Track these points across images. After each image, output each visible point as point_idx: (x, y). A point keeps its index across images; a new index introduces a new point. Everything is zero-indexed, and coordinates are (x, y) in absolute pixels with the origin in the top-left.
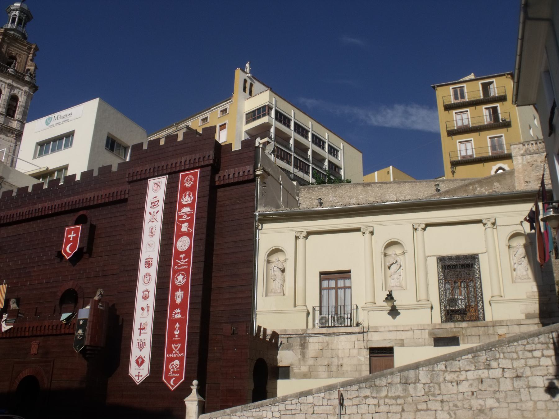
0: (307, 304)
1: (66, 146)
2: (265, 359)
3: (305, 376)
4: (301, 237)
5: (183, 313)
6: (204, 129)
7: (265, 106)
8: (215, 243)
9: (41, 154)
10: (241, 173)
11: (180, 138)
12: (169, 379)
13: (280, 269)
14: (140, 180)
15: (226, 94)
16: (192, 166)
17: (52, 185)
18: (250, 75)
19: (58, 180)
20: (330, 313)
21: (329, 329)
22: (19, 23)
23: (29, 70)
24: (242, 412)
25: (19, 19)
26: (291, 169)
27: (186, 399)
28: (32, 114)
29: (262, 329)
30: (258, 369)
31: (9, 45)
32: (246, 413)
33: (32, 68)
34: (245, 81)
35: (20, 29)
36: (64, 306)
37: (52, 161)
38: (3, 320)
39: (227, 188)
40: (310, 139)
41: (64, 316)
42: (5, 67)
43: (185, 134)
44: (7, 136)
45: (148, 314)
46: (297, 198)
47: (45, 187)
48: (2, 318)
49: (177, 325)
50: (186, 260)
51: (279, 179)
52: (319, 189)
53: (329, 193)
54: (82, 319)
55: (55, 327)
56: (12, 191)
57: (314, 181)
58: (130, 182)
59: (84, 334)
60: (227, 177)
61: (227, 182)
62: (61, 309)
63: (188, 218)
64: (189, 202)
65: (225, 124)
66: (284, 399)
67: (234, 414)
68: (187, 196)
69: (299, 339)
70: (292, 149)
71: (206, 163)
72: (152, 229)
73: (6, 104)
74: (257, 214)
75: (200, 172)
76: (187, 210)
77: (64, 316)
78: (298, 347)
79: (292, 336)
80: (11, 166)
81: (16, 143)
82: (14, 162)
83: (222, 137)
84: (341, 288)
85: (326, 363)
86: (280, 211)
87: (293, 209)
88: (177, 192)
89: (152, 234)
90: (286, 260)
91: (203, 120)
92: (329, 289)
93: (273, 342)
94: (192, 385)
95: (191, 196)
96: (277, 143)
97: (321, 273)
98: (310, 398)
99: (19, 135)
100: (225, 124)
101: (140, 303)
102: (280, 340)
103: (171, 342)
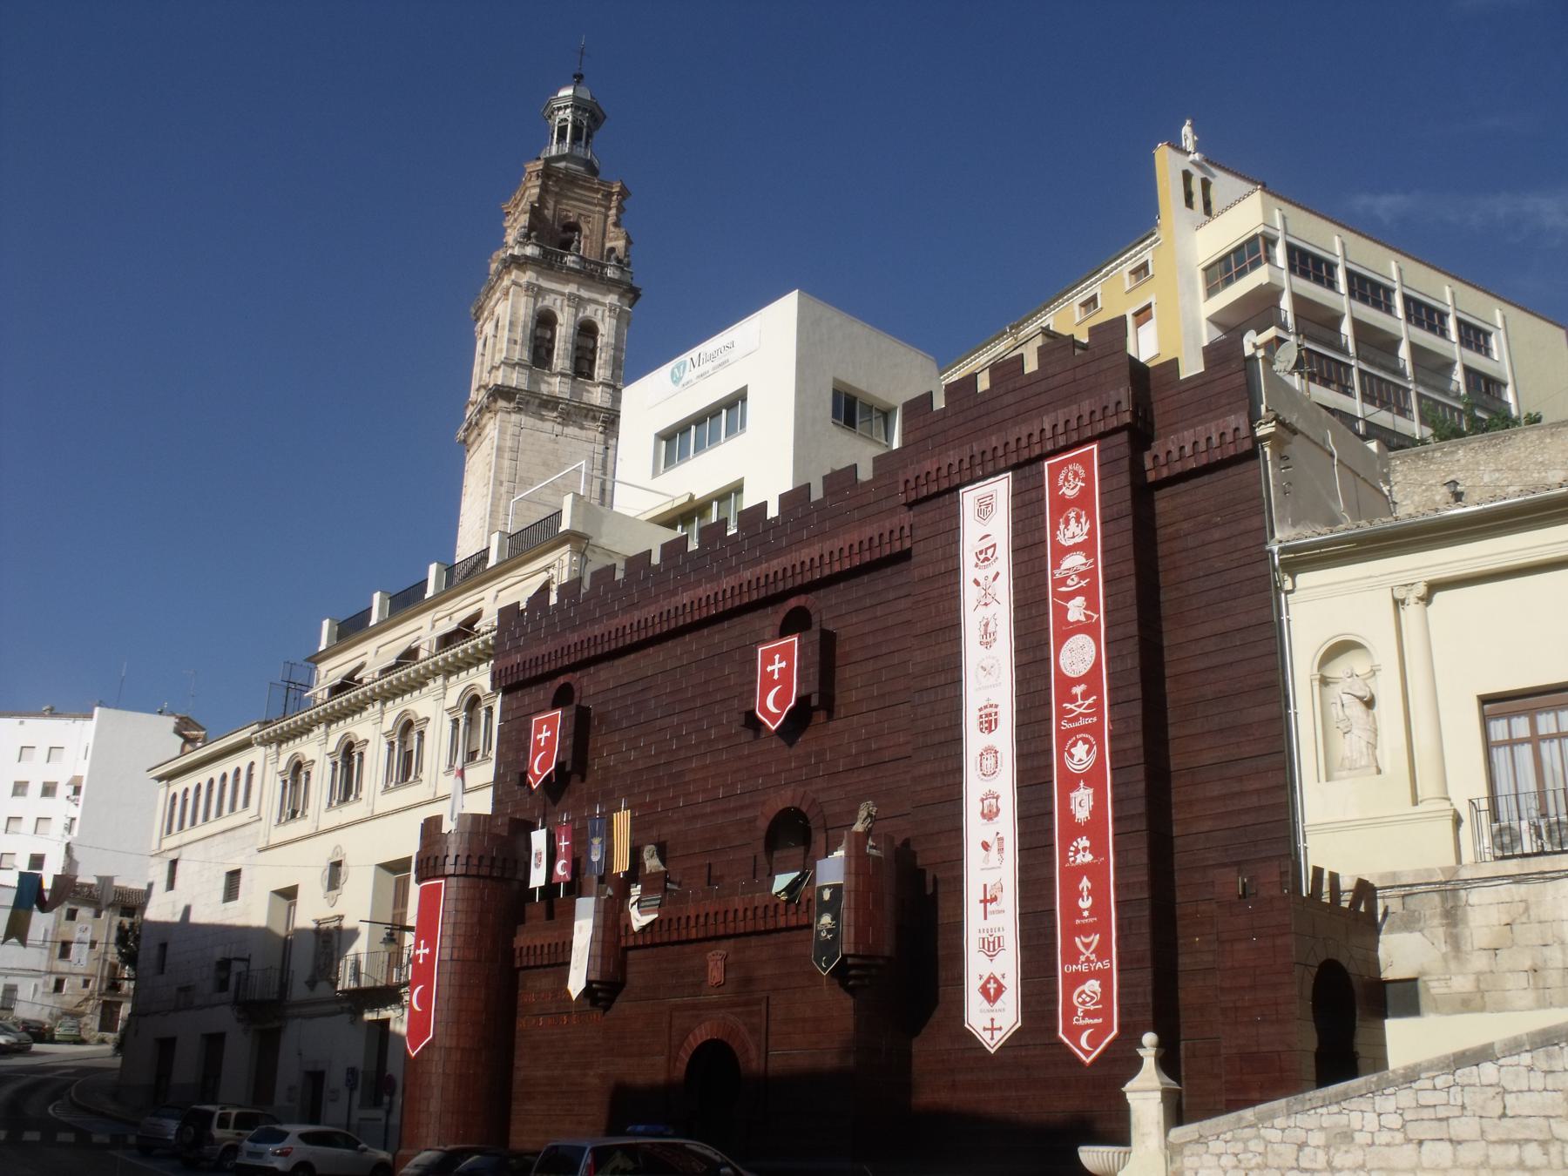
0: (1451, 795)
1: (731, 431)
2: (1344, 961)
3: (1466, 1004)
4: (1412, 598)
5: (1098, 848)
6: (1093, 331)
7: (1255, 237)
8: (1165, 643)
9: (670, 462)
10: (1215, 440)
11: (1031, 365)
12: (1074, 1032)
13: (1361, 699)
14: (939, 494)
15: (1135, 219)
16: (1075, 437)
17: (714, 540)
18: (1197, 157)
19: (723, 523)
20: (1524, 814)
21: (1525, 860)
22: (576, 138)
23: (612, 250)
24: (1289, 1115)
25: (575, 127)
26: (1355, 405)
27: (1129, 1086)
28: (631, 367)
29: (1326, 876)
30: (1302, 997)
31: (559, 196)
32: (1300, 1119)
33: (620, 244)
34: (1187, 176)
35: (579, 151)
36: (776, 855)
37: (699, 476)
38: (632, 900)
39: (1182, 486)
40: (1453, 334)
41: (781, 881)
42: (557, 254)
43: (1042, 352)
44: (582, 428)
45: (1002, 860)
46: (1385, 489)
47: (693, 545)
48: (629, 896)
49: (1085, 883)
50: (1090, 701)
51: (1325, 440)
52: (1445, 454)
53: (1478, 463)
54: (829, 887)
55: (760, 912)
56: (612, 569)
57: (1428, 431)
58: (910, 505)
59: (837, 925)
60: (1175, 455)
61: (1178, 468)
62: (770, 864)
63: (1083, 583)
64: (1079, 540)
65: (1149, 306)
66: (1411, 1076)
67: (1268, 1124)
68: (1073, 522)
69: (1436, 898)
70: (1351, 349)
71: (1114, 423)
72: (987, 625)
73: (570, 347)
74: (1276, 549)
75: (1100, 451)
76: (1075, 561)
77: (781, 881)
78: (1436, 921)
79: (1415, 890)
80: (602, 504)
81: (606, 442)
82: (608, 493)
83: (1145, 346)
84: (1550, 737)
85: (1528, 964)
86: (1340, 531)
87: (1376, 521)
88: (1044, 513)
89: (987, 639)
90: (1373, 673)
91: (1084, 305)
92: (1512, 743)
93: (1360, 912)
94: (1142, 1046)
95: (1083, 520)
96: (1308, 337)
97: (1485, 700)
98: (1488, 1071)
99: (610, 421)
100: (1149, 306)
101: (975, 829)
102: (1380, 902)
103: (1072, 931)
